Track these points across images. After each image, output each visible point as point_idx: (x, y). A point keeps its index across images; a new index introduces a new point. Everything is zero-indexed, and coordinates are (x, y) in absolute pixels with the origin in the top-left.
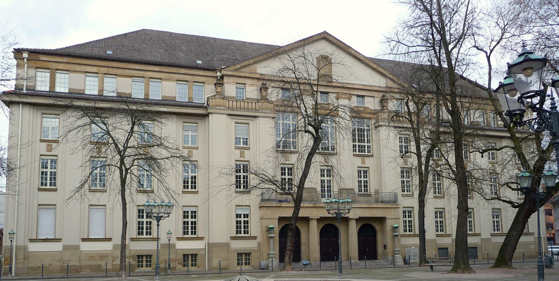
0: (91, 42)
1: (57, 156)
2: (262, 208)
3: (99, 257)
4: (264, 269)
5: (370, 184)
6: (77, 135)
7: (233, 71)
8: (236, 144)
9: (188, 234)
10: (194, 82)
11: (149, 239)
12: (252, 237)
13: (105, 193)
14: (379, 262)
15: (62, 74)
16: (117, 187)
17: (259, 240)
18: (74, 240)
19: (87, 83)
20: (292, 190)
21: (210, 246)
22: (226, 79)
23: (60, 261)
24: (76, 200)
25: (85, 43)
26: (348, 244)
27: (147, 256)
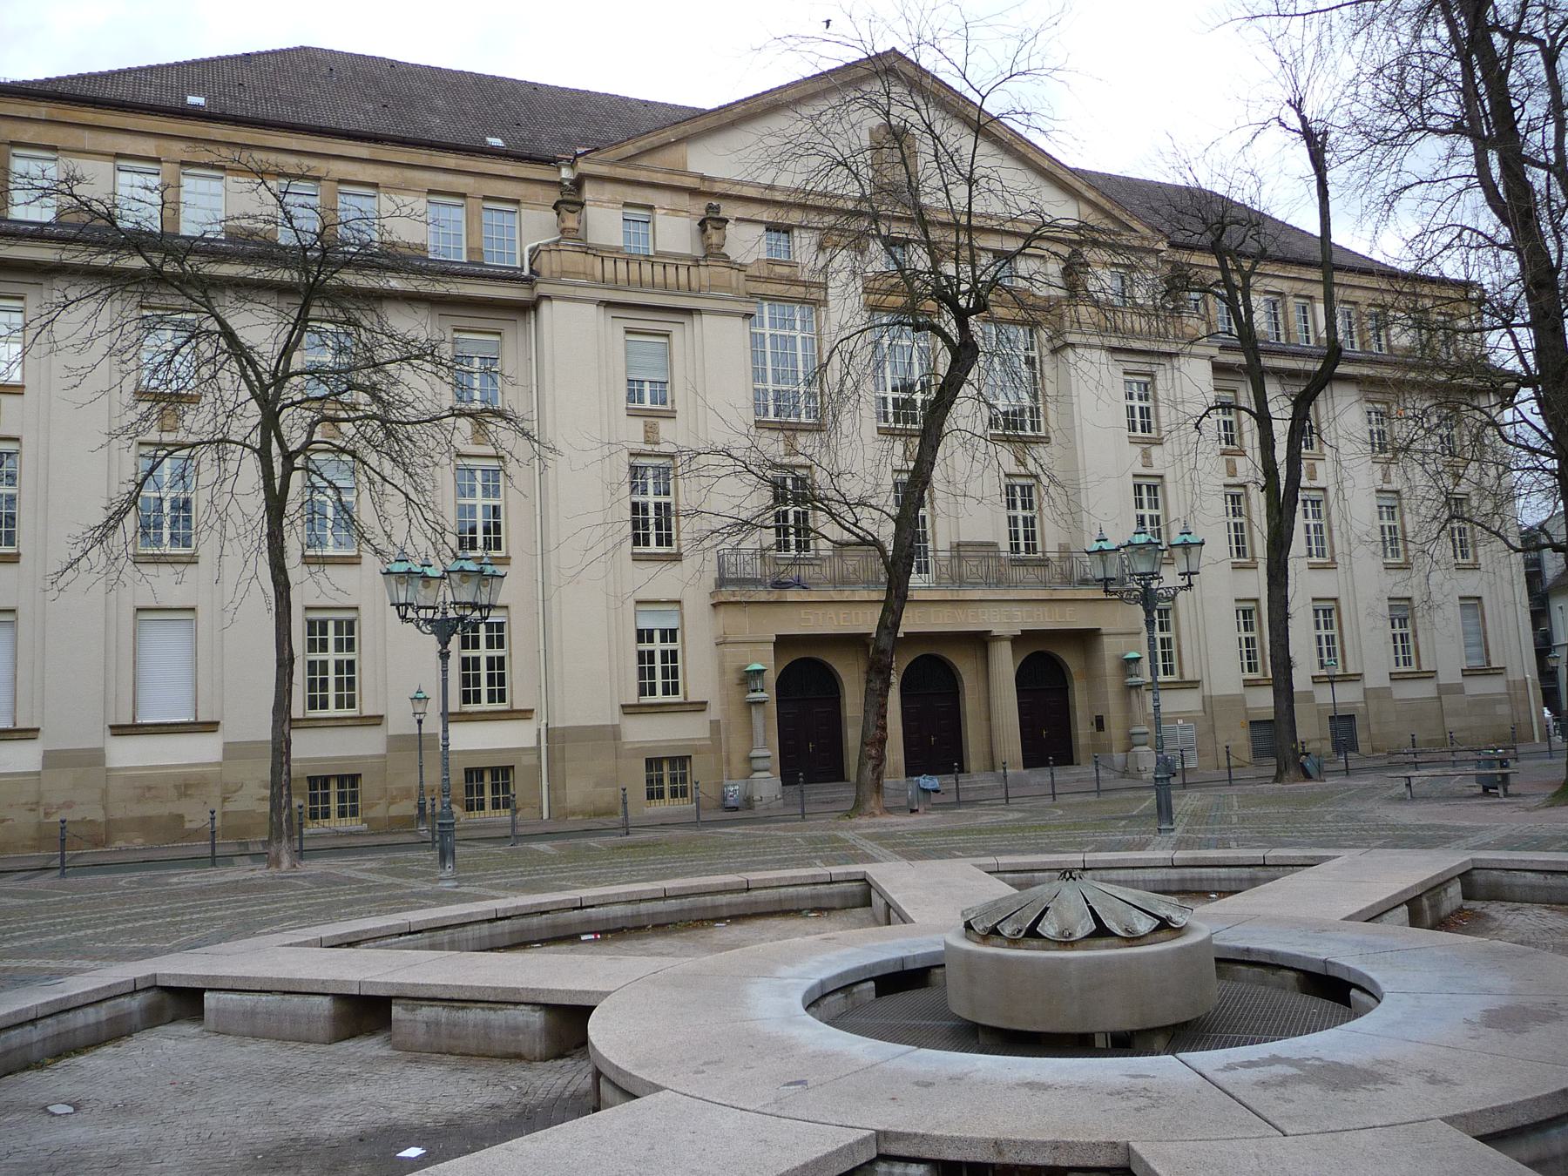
0: (130, 70)
1: (17, 440)
2: (722, 609)
3: (176, 787)
4: (736, 809)
5: (1042, 529)
6: (91, 323)
7: (612, 164)
8: (630, 399)
9: (478, 700)
10: (486, 198)
11: (349, 722)
12: (691, 703)
13: (190, 566)
14: (1083, 771)
16: (249, 527)
17: (714, 712)
18: (89, 735)
20: (807, 549)
21: (556, 737)
22: (589, 192)
23: (33, 807)
24: (93, 577)
25: (112, 73)
26: (989, 719)
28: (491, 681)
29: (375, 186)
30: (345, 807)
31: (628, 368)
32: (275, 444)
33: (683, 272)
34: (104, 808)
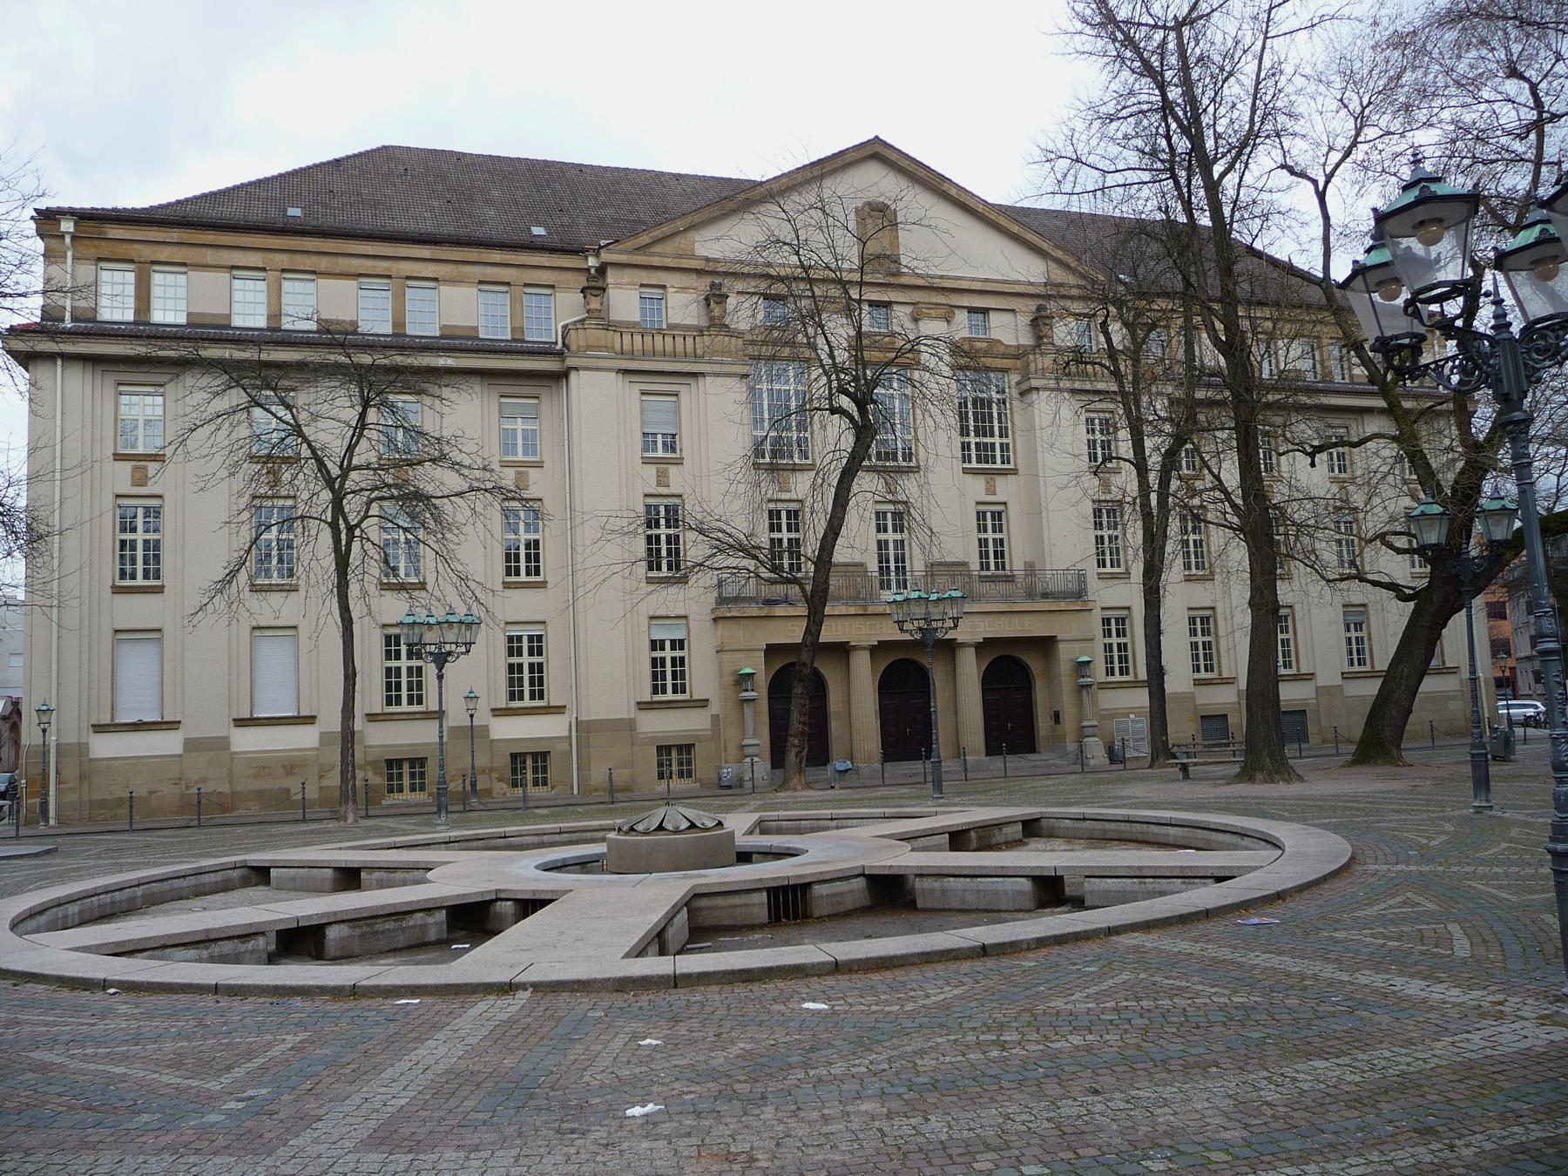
0: (243, 185)
1: (160, 497)
2: (721, 621)
4: (730, 787)
6: (213, 438)
7: (630, 253)
8: (645, 449)
9: (521, 698)
10: (526, 285)
17: (715, 708)
18: (222, 728)
20: (799, 570)
21: (584, 728)
22: (612, 276)
24: (216, 616)
26: (956, 713)
27: (412, 761)
28: (532, 683)
29: (436, 280)
31: (643, 423)
32: (341, 522)
33: (689, 341)
34: (230, 783)
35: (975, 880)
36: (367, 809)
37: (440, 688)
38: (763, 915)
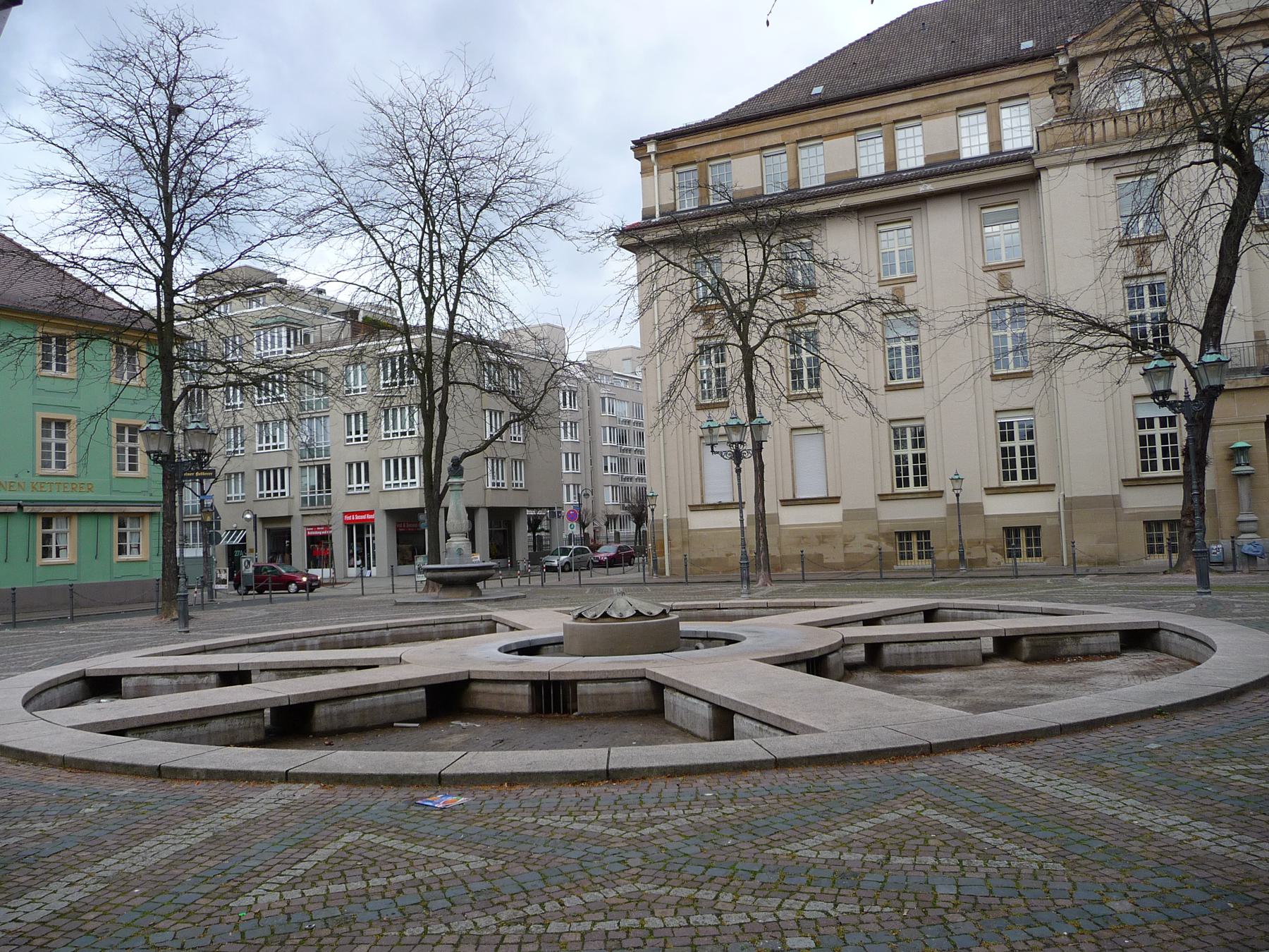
3: (818, 537)
11: (920, 496)
15: (971, 117)
19: (964, 133)
27: (919, 534)
29: (919, 117)
30: (1036, 545)
35: (689, 699)
36: (881, 573)
37: (739, 480)
38: (525, 705)
